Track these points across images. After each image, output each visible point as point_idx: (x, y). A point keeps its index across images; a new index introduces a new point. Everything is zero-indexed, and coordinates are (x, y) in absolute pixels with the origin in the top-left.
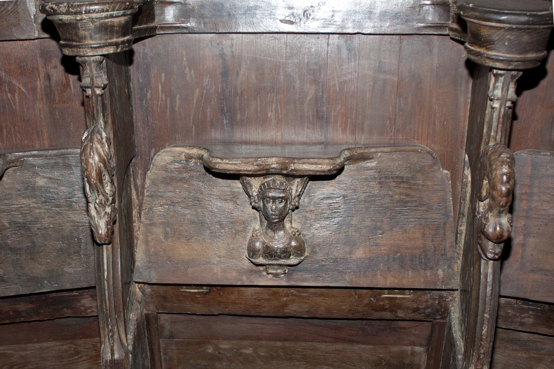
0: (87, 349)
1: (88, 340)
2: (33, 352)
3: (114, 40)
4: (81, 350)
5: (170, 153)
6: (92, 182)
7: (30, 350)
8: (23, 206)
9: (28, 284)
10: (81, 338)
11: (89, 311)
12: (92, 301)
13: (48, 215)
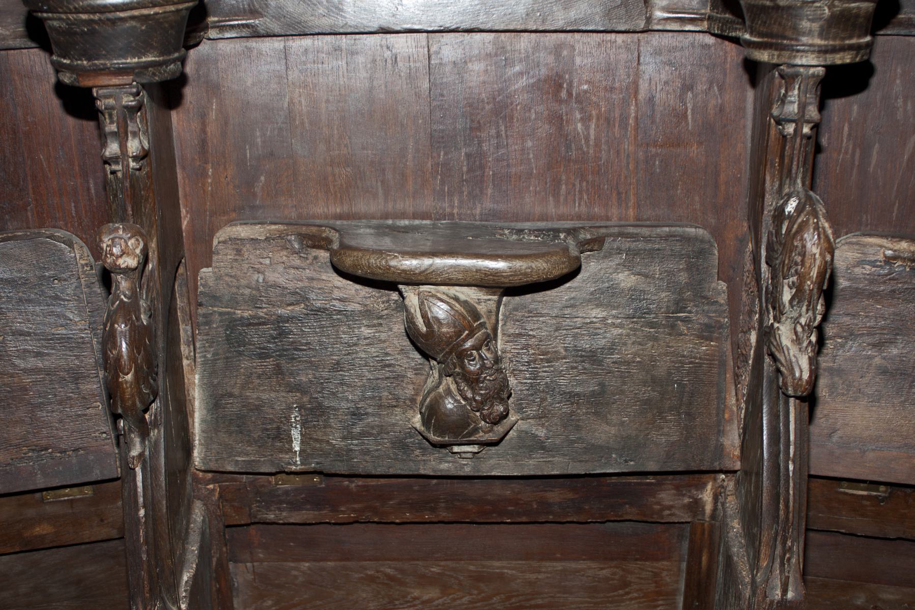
0: (641, 579)
1: (647, 563)
2: (549, 575)
3: (854, 41)
4: (632, 580)
5: (857, 247)
6: (806, 287)
7: (545, 573)
8: (594, 320)
9: (584, 456)
10: (637, 560)
11: (667, 512)
12: (675, 495)
13: (633, 339)
